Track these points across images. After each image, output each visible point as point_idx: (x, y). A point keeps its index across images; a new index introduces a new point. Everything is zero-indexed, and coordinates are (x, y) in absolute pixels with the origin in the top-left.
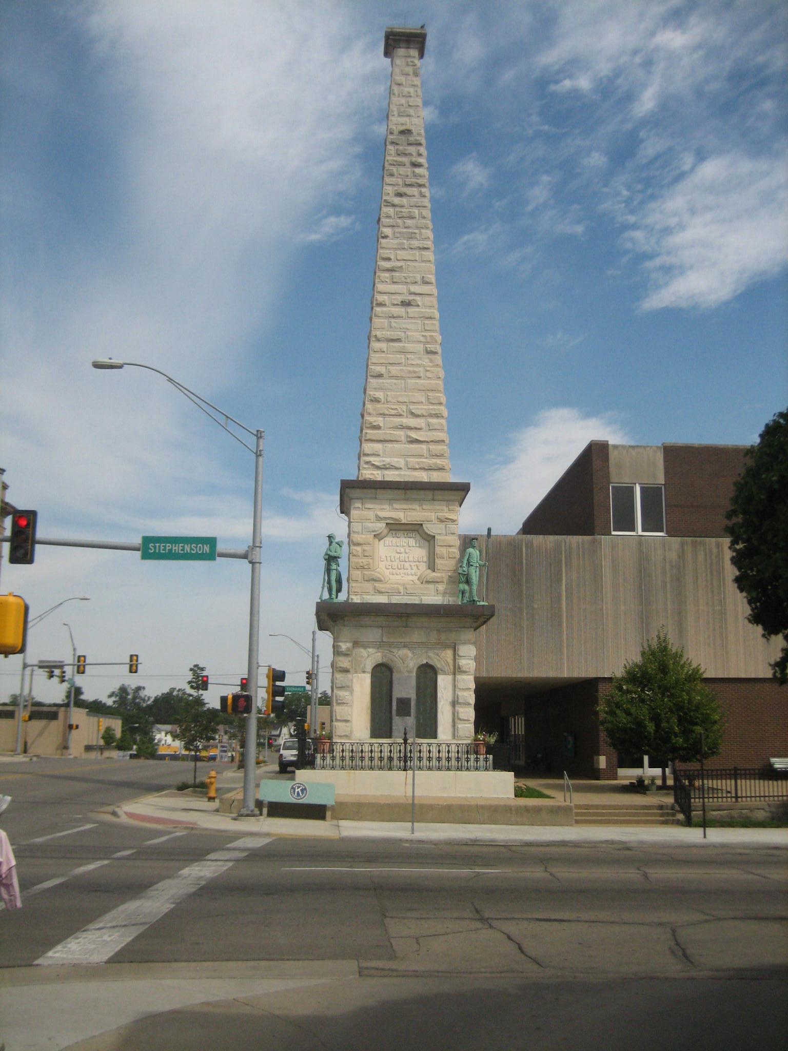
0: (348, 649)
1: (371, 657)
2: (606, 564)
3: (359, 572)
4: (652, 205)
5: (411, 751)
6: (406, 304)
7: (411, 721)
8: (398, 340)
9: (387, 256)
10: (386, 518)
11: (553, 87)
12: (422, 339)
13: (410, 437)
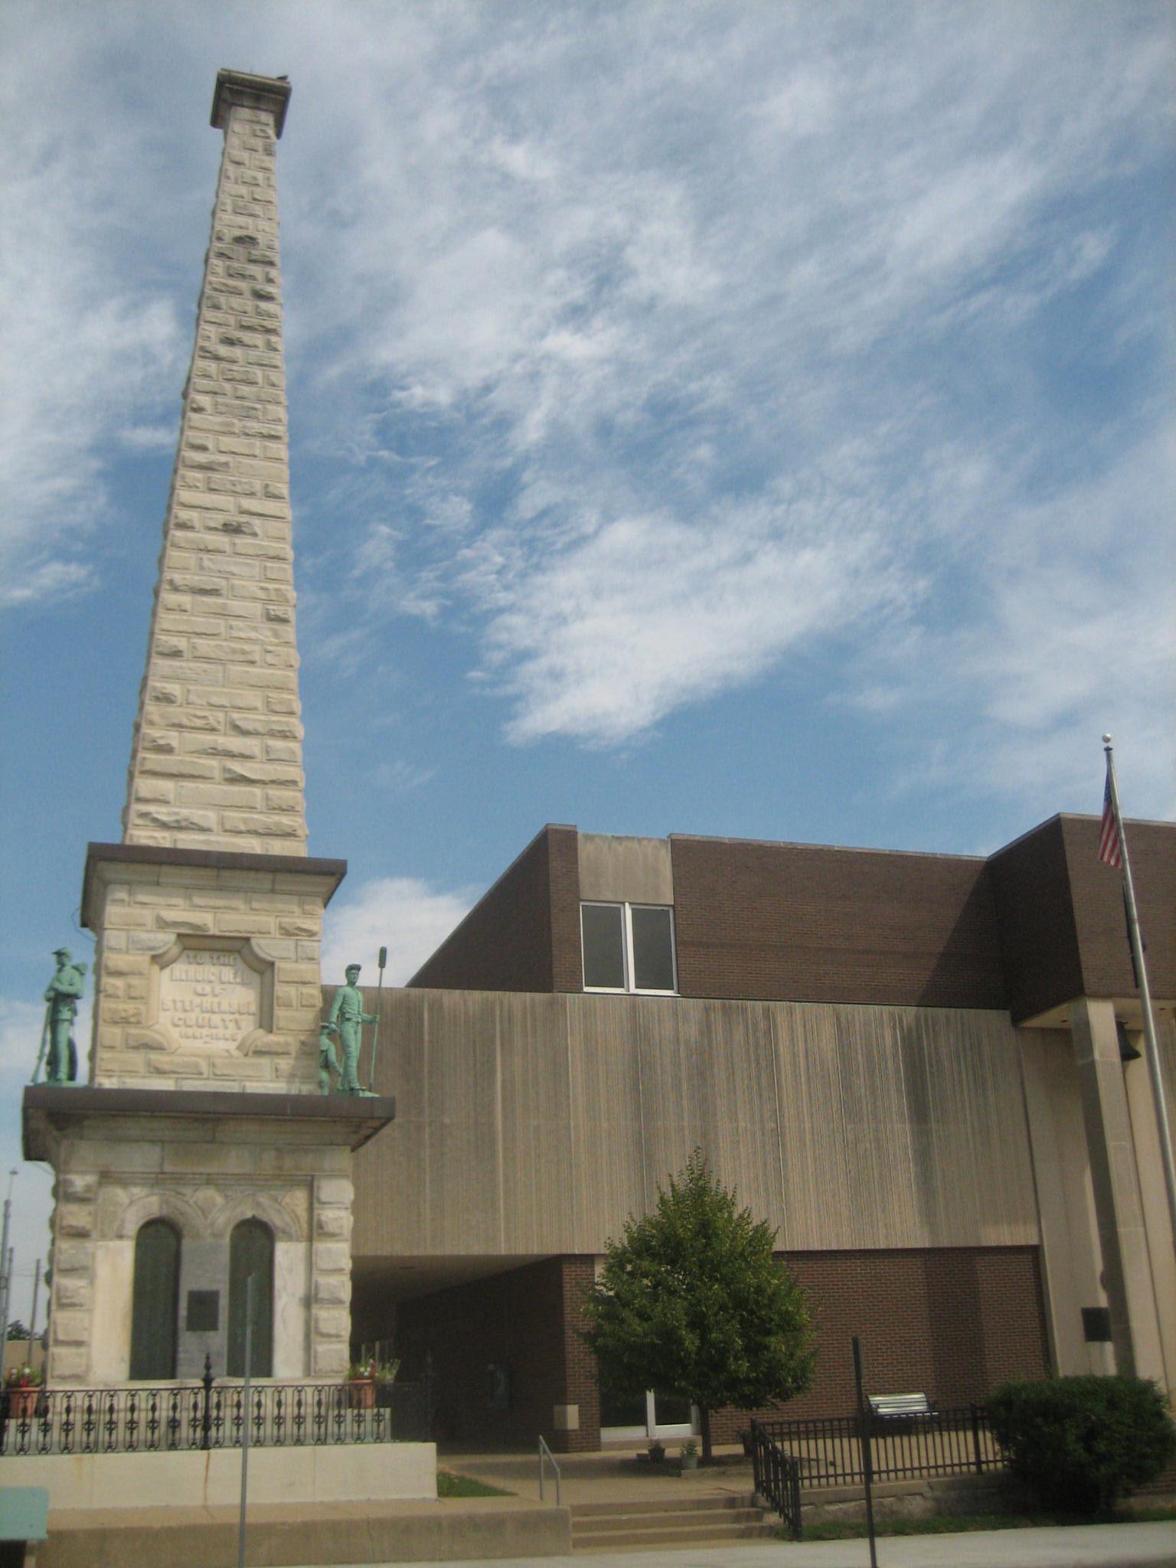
0: (88, 1188)
1: (136, 1205)
2: (574, 1043)
3: (117, 1031)
4: (539, 579)
5: (218, 1406)
6: (232, 529)
7: (218, 1340)
8: (214, 592)
9: (198, 442)
10: (175, 924)
11: (399, 395)
12: (261, 594)
13: (229, 771)
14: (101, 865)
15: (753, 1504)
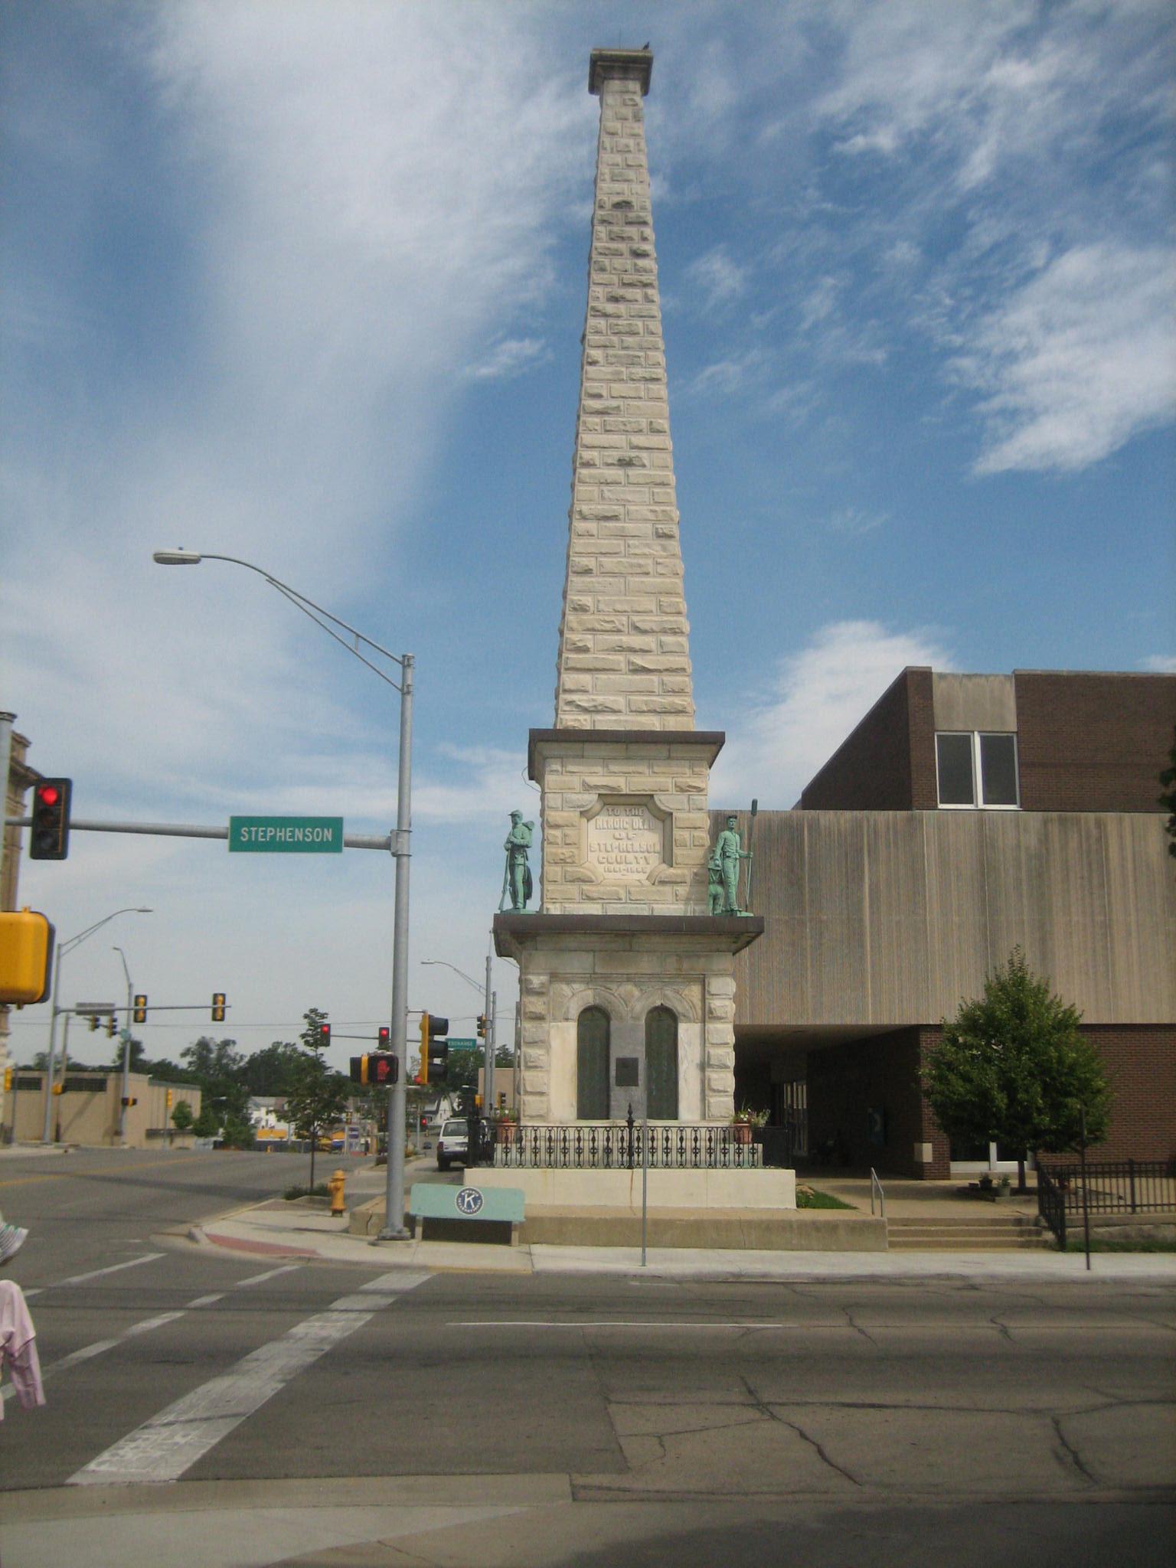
1: (577, 997)
2: (931, 852)
3: (558, 869)
4: (988, 319)
5: (638, 1139)
6: (625, 463)
7: (639, 1093)
8: (614, 518)
9: (595, 391)
10: (596, 787)
12: (651, 516)
13: (633, 663)
14: (540, 745)
15: (1036, 1224)
